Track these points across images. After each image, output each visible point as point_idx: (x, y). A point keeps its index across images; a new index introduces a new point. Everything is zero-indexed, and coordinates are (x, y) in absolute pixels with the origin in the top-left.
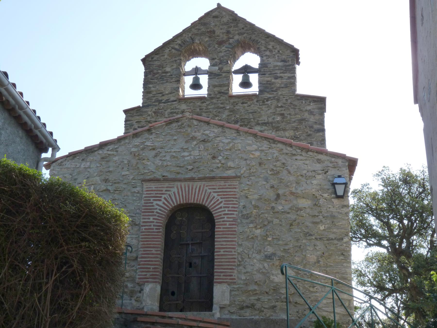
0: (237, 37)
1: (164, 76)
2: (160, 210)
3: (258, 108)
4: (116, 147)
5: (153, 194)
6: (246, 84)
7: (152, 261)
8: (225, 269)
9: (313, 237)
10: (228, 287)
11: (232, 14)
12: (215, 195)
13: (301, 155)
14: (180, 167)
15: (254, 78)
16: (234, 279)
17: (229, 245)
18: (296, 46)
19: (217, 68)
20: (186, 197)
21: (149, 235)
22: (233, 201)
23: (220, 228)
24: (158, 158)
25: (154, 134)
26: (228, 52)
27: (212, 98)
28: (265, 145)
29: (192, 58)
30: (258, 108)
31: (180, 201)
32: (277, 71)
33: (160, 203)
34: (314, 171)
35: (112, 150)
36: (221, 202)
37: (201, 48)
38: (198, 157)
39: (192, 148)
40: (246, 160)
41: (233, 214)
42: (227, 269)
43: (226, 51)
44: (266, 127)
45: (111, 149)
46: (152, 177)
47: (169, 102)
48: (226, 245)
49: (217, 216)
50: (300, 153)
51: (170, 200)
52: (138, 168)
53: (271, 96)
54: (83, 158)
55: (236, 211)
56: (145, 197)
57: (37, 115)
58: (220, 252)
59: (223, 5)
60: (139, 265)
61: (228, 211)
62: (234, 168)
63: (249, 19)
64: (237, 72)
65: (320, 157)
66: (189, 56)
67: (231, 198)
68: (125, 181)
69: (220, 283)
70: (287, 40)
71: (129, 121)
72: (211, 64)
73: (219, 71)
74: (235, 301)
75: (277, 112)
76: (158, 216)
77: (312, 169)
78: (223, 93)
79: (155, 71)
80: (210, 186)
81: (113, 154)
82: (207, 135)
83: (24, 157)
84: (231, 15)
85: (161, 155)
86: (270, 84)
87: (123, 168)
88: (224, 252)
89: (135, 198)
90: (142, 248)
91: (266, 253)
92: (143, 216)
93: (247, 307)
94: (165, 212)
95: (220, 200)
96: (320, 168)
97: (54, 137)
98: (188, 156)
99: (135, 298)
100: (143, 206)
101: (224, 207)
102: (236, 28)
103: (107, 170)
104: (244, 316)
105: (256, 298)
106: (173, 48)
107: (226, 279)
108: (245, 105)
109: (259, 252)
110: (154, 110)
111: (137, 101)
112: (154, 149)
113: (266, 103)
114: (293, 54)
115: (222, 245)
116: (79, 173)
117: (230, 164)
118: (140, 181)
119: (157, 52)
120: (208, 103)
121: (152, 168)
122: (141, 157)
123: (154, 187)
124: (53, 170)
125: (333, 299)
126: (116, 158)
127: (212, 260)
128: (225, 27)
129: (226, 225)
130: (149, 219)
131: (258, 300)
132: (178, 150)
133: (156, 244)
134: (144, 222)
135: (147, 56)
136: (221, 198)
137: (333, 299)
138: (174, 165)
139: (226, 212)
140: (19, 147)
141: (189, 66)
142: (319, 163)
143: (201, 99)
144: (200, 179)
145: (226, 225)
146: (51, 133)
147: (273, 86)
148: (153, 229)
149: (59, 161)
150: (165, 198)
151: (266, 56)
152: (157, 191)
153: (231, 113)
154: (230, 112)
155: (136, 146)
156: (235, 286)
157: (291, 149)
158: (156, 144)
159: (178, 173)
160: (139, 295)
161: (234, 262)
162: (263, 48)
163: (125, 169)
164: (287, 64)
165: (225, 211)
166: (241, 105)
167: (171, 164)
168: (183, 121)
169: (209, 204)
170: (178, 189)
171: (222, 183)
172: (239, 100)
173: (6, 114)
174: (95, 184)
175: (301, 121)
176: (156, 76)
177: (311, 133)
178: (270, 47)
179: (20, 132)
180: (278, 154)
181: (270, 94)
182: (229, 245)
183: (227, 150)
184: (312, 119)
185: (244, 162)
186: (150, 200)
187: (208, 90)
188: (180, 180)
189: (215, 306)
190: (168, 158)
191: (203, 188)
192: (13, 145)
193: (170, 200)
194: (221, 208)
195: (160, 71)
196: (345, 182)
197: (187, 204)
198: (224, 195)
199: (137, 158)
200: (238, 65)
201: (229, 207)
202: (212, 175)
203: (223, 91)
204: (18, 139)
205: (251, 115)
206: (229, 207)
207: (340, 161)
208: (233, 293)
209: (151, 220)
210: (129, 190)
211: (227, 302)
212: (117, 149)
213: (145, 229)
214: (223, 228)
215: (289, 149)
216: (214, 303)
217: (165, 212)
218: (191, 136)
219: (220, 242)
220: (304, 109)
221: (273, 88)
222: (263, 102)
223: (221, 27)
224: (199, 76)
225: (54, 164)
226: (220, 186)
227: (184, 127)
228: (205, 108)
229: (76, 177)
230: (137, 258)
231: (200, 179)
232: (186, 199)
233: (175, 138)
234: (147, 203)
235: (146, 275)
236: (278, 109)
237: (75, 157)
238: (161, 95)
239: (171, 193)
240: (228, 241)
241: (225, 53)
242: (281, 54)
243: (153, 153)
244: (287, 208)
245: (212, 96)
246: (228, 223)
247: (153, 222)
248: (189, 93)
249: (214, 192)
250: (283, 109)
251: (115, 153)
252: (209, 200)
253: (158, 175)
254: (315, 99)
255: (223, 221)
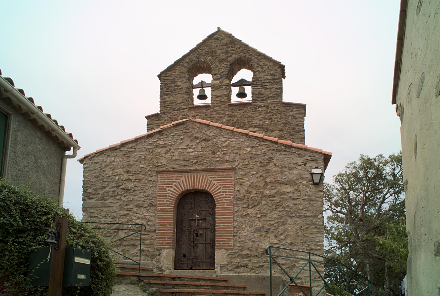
0: (234, 56)
1: (176, 89)
2: (172, 194)
3: (252, 113)
4: (134, 145)
5: (165, 182)
6: (242, 95)
7: (167, 233)
8: (224, 239)
9: (294, 215)
10: (226, 252)
11: (230, 36)
12: (215, 182)
13: (285, 151)
14: (186, 161)
15: (248, 90)
16: (231, 246)
17: (226, 221)
18: (283, 63)
19: (218, 82)
20: (192, 184)
21: (164, 213)
22: (229, 187)
23: (220, 208)
24: (169, 154)
25: (164, 135)
26: (227, 68)
27: (215, 106)
28: (255, 143)
29: (199, 74)
30: (252, 113)
31: (187, 187)
32: (266, 84)
33: (172, 189)
34: (296, 163)
35: (131, 148)
36: (220, 188)
37: (205, 65)
38: (201, 153)
39: (196, 145)
40: (240, 155)
41: (230, 197)
42: (226, 238)
43: (225, 68)
44: (258, 129)
45: (130, 147)
46: (164, 169)
47: (181, 109)
48: (225, 220)
49: (216, 199)
50: (284, 149)
51: (179, 187)
52: (153, 162)
53: (261, 104)
54: (108, 154)
55: (232, 195)
56: (160, 184)
57: (53, 118)
58: (220, 226)
59: (223, 29)
60: (157, 236)
61: (226, 195)
62: (230, 161)
63: (244, 41)
64: (235, 85)
65: (300, 152)
66: (196, 73)
67: (227, 185)
68: (143, 172)
69: (220, 249)
70: (275, 58)
71: (150, 125)
72: (213, 78)
73: (220, 84)
74: (232, 262)
75: (267, 117)
76: (170, 199)
77: (294, 162)
78: (223, 102)
79: (169, 85)
80: (211, 175)
81: (132, 151)
82: (207, 135)
83: (46, 155)
84: (229, 37)
85: (171, 151)
86: (260, 94)
87: (141, 162)
88: (223, 226)
89: (151, 185)
90: (158, 223)
91: (256, 227)
92: (159, 199)
93: (241, 266)
94: (175, 196)
95: (220, 187)
96: (300, 161)
97: (74, 138)
98: (192, 152)
99: (155, 259)
100: (158, 191)
101: (223, 192)
102: (234, 48)
103: (128, 163)
104: (239, 273)
105: (248, 259)
106: (182, 66)
107: (224, 246)
108: (241, 111)
109: (251, 226)
110: (169, 116)
111: (156, 109)
112: (165, 147)
113: (258, 109)
114: (280, 70)
115: (221, 221)
116: (106, 166)
117: (227, 158)
118: (155, 172)
119: (170, 68)
120: (211, 110)
121: (164, 161)
122: (154, 153)
123: (166, 176)
124: (86, 164)
125: (310, 270)
126: (134, 154)
127: (213, 231)
128: (225, 47)
129: (224, 205)
130: (164, 201)
131: (250, 261)
132: (184, 147)
133: (169, 220)
134: (159, 204)
135: (162, 73)
136: (220, 185)
137: (310, 270)
138: (182, 159)
139: (224, 196)
140: (39, 147)
141: (196, 80)
142: (300, 157)
143: (206, 107)
144: (203, 171)
145: (224, 205)
146: (71, 135)
147: (263, 96)
148: (167, 209)
149: (90, 157)
150: (175, 185)
151: (258, 71)
152: (169, 179)
153: (230, 118)
154: (229, 117)
155: (150, 144)
156: (232, 251)
157: (277, 146)
158: (166, 142)
159: (185, 166)
160: (158, 257)
161: (231, 233)
162: (256, 65)
163: (143, 162)
164: (275, 78)
165: (223, 195)
166: (238, 111)
167: (179, 158)
168: (188, 124)
169: (210, 190)
170: (185, 178)
171: (221, 173)
172: (236, 107)
173: (20, 118)
174: (119, 175)
175: (286, 124)
176: (170, 89)
177: (294, 133)
178: (261, 64)
179: (39, 133)
180: (266, 150)
181: (261, 102)
182: (226, 221)
183: (224, 147)
184: (294, 123)
185: (238, 156)
186: (163, 187)
187: (211, 100)
188: (187, 171)
189: (216, 266)
190: (176, 154)
191: (206, 177)
192: (32, 145)
193: (179, 187)
194: (220, 192)
195: (172, 85)
196: (321, 172)
197: (193, 189)
198: (222, 182)
199: (152, 154)
200: (235, 79)
201: (226, 192)
202: (213, 167)
203: (223, 100)
204: (37, 140)
205: (246, 119)
206: (226, 192)
207: (317, 156)
208: (230, 256)
209: (165, 202)
210: (147, 179)
211: (226, 263)
212: (135, 147)
213: (161, 209)
214: (222, 208)
215: (275, 145)
216: (216, 263)
217: (175, 196)
218: (194, 136)
219: (220, 218)
220: (288, 114)
221: (263, 97)
222: (256, 109)
223: (221, 47)
224: (204, 88)
225: (86, 159)
226: (219, 175)
227: (189, 129)
228: (209, 114)
229: (104, 169)
230: (155, 230)
231: (203, 171)
232: (192, 186)
233: (182, 137)
234: (161, 189)
235: (163, 243)
236: (268, 115)
237: (102, 153)
238: (174, 104)
239: (180, 181)
240: (226, 218)
241: (225, 69)
242: (270, 70)
243: (164, 150)
244: (273, 192)
245: (215, 104)
246: (225, 204)
247: (167, 204)
248: (197, 102)
249: (214, 180)
250: (271, 114)
251: (133, 150)
252: (210, 186)
253: (169, 168)
254: (297, 106)
255: (222, 203)
